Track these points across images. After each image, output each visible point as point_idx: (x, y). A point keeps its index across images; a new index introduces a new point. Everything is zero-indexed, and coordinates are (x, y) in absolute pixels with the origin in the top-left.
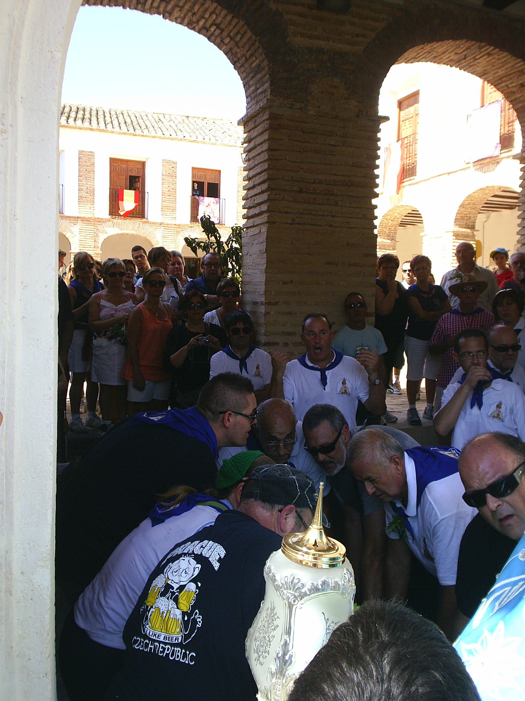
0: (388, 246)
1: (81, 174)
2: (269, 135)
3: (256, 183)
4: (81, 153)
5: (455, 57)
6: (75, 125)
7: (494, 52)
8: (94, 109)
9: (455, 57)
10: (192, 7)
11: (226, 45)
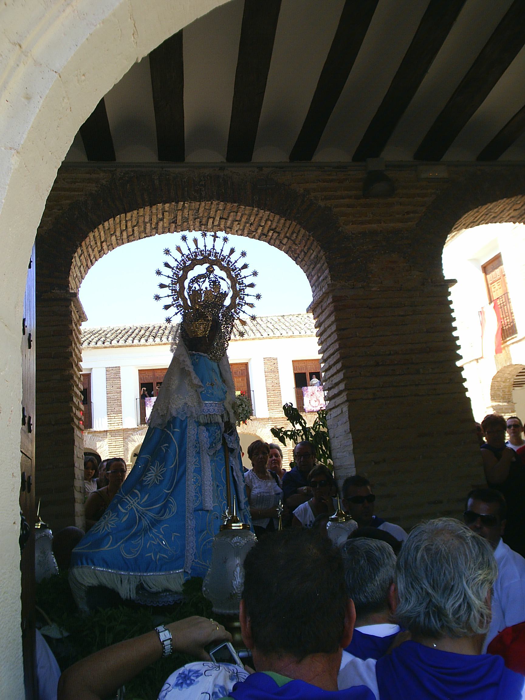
0: (506, 409)
2: (335, 316)
3: (332, 363)
10: (248, 219)
11: (285, 245)
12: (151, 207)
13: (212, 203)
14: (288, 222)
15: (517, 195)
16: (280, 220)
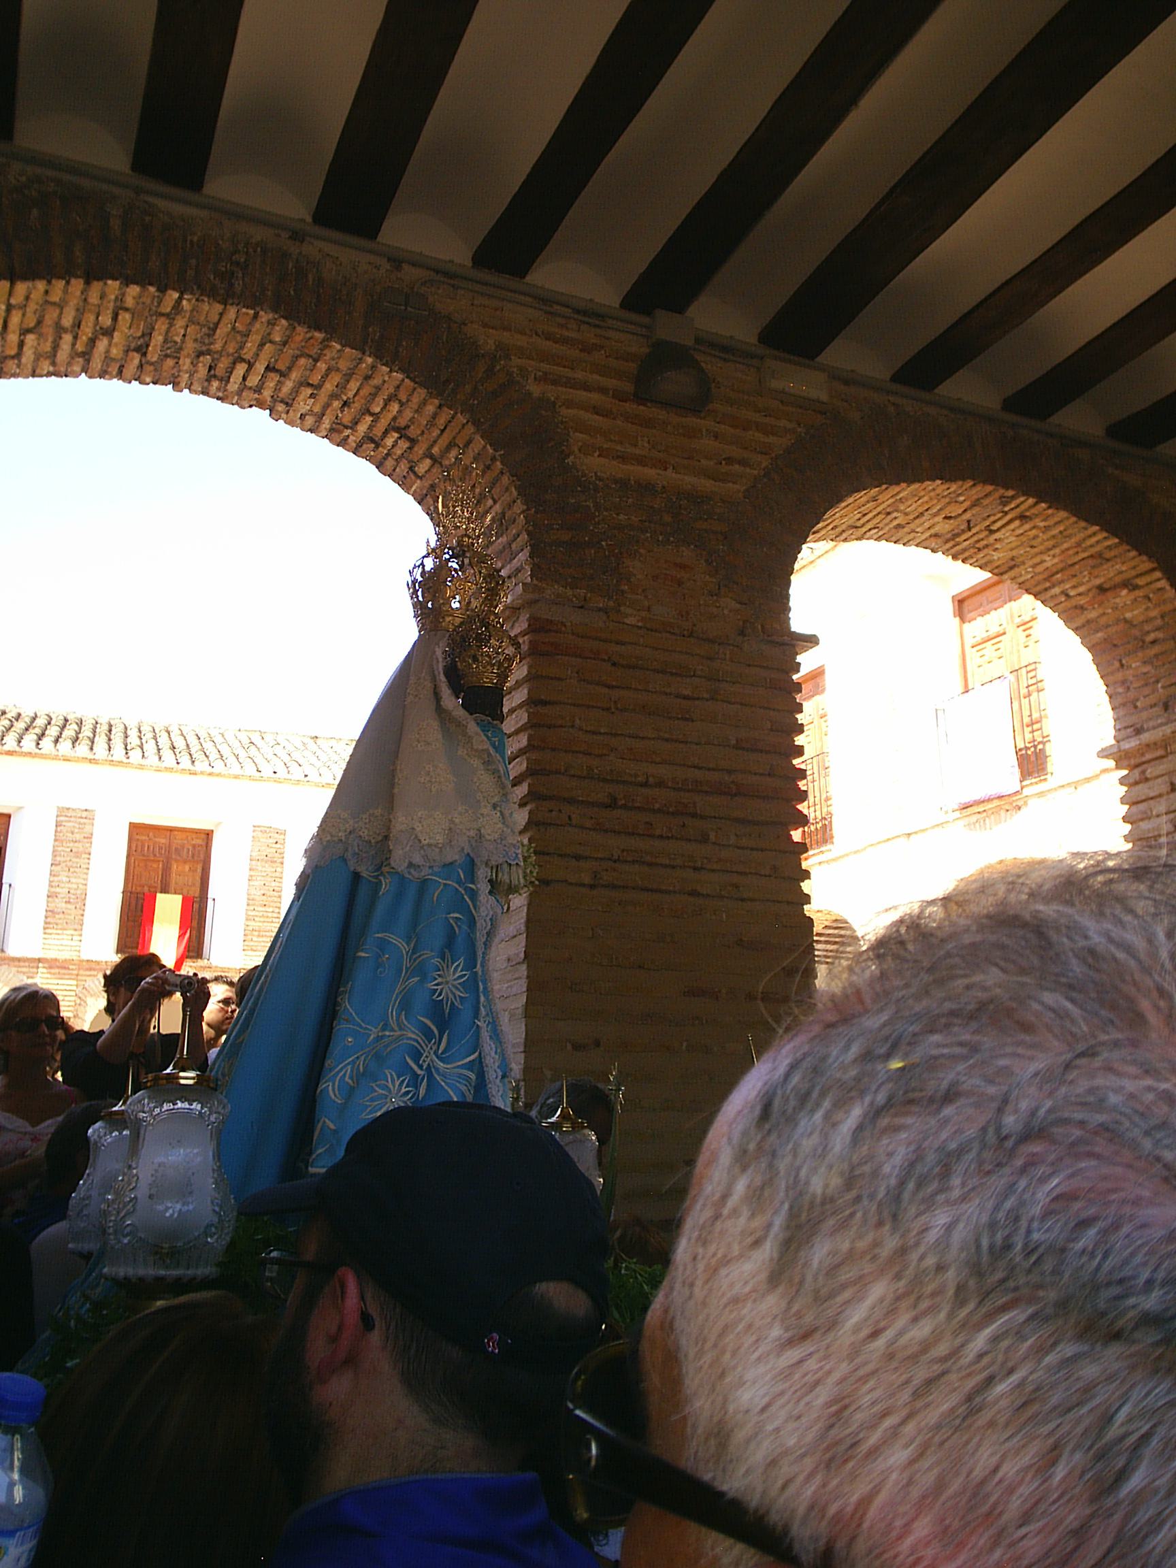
1: (58, 858)
2: (530, 667)
4: (63, 812)
5: (943, 527)
6: (54, 752)
7: (1034, 511)
8: (103, 721)
9: (943, 527)
10: (342, 387)
11: (421, 478)
12: (88, 283)
13: (256, 316)
14: (447, 413)
15: (964, 479)
16: (424, 403)
